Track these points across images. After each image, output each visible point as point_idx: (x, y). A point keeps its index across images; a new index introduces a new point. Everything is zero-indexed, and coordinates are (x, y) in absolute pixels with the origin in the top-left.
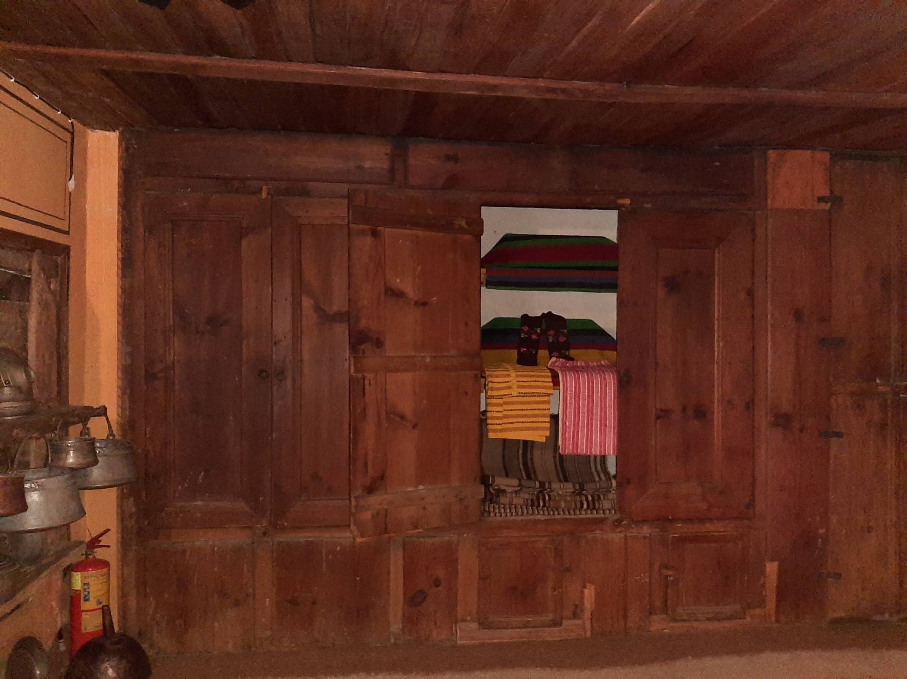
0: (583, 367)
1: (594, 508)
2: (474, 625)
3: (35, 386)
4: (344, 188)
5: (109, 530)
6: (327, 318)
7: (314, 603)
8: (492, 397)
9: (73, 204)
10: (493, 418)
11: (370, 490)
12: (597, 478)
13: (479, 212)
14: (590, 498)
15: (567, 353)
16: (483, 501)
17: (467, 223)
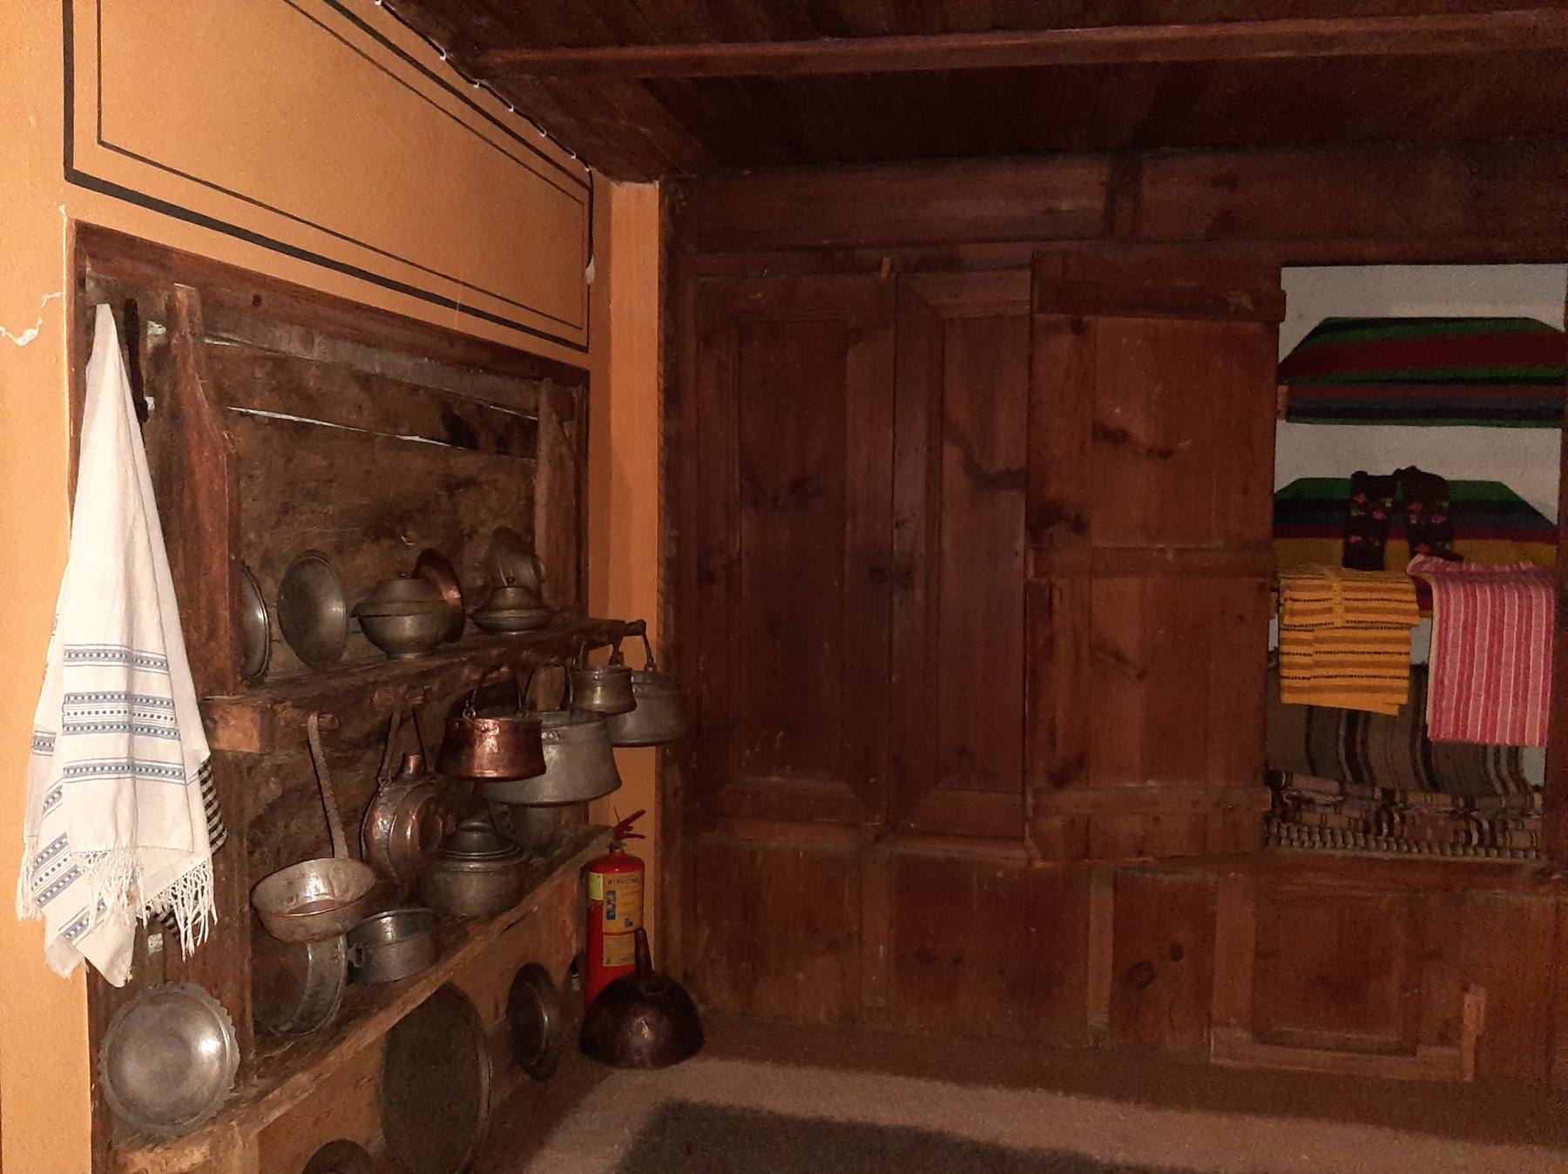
0: (1480, 574)
1: (1494, 844)
2: (1244, 1035)
3: (545, 586)
4: (1024, 250)
5: (642, 813)
6: (987, 482)
7: (957, 962)
8: (1290, 628)
9: (593, 300)
10: (1291, 666)
11: (1060, 780)
12: (1500, 791)
13: (1277, 279)
14: (1486, 825)
15: (1448, 547)
16: (1268, 819)
17: (1255, 302)
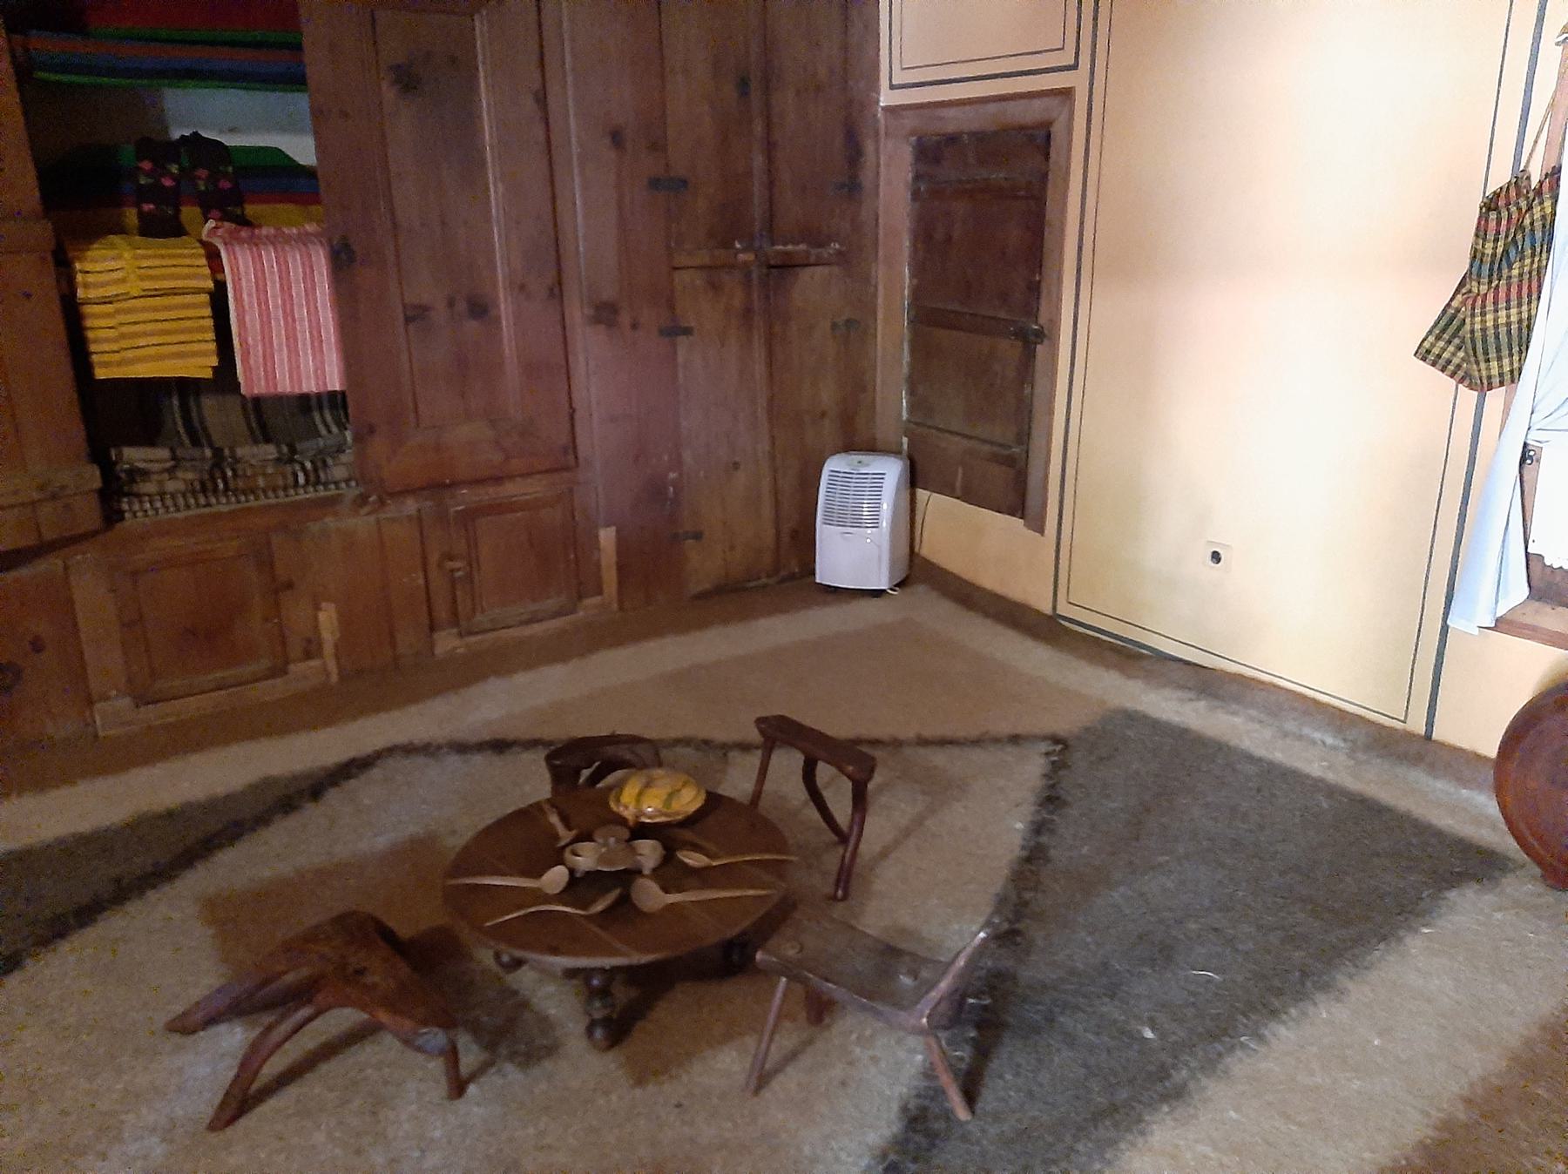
1: (318, 482)
14: (308, 465)
